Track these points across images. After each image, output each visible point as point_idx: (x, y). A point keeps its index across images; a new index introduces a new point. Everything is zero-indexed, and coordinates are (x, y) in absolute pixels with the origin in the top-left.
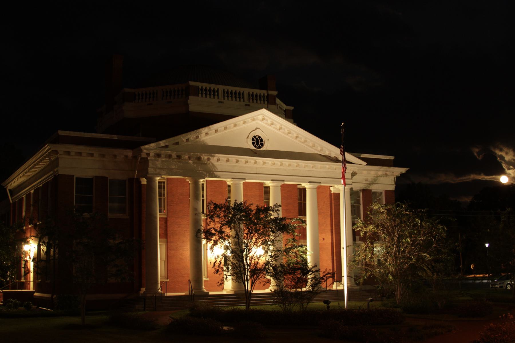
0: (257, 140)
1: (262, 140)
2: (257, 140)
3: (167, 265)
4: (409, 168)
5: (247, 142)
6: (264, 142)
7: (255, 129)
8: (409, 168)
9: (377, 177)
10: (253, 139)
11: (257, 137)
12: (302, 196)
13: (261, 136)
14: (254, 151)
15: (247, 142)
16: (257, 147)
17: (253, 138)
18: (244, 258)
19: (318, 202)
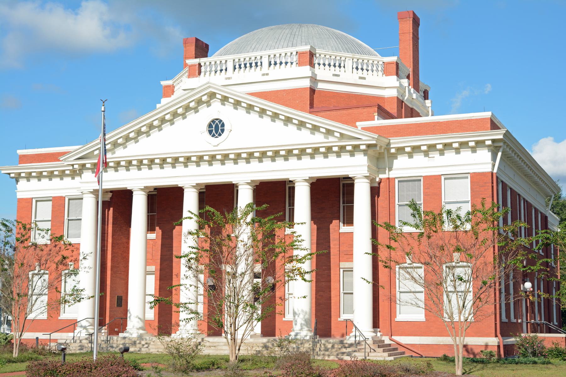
0: (217, 131)
1: (210, 132)
2: (217, 131)
3: (343, 279)
4: (59, 318)
5: (231, 125)
6: (208, 129)
7: (216, 145)
8: (59, 318)
9: (423, 372)
10: (223, 131)
11: (217, 135)
12: (397, 357)
13: (213, 138)
14: (388, 116)
15: (231, 125)
16: (217, 121)
17: (223, 133)
18: (543, 261)
19: (379, 290)
